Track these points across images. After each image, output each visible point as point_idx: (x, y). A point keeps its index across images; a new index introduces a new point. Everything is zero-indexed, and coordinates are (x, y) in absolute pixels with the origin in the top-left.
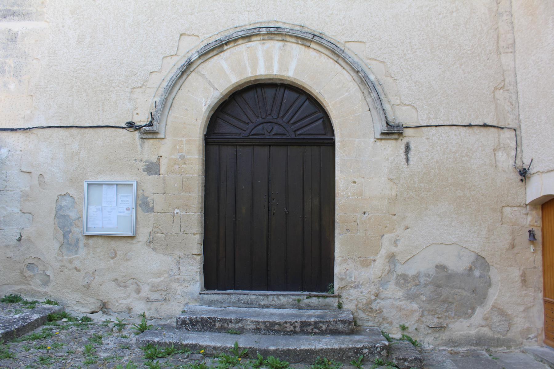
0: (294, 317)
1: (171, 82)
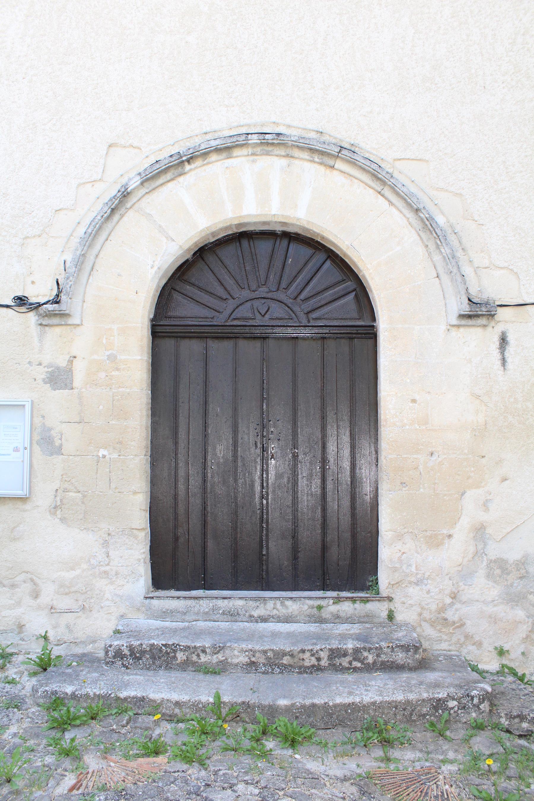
0: (315, 641)
1: (92, 227)
